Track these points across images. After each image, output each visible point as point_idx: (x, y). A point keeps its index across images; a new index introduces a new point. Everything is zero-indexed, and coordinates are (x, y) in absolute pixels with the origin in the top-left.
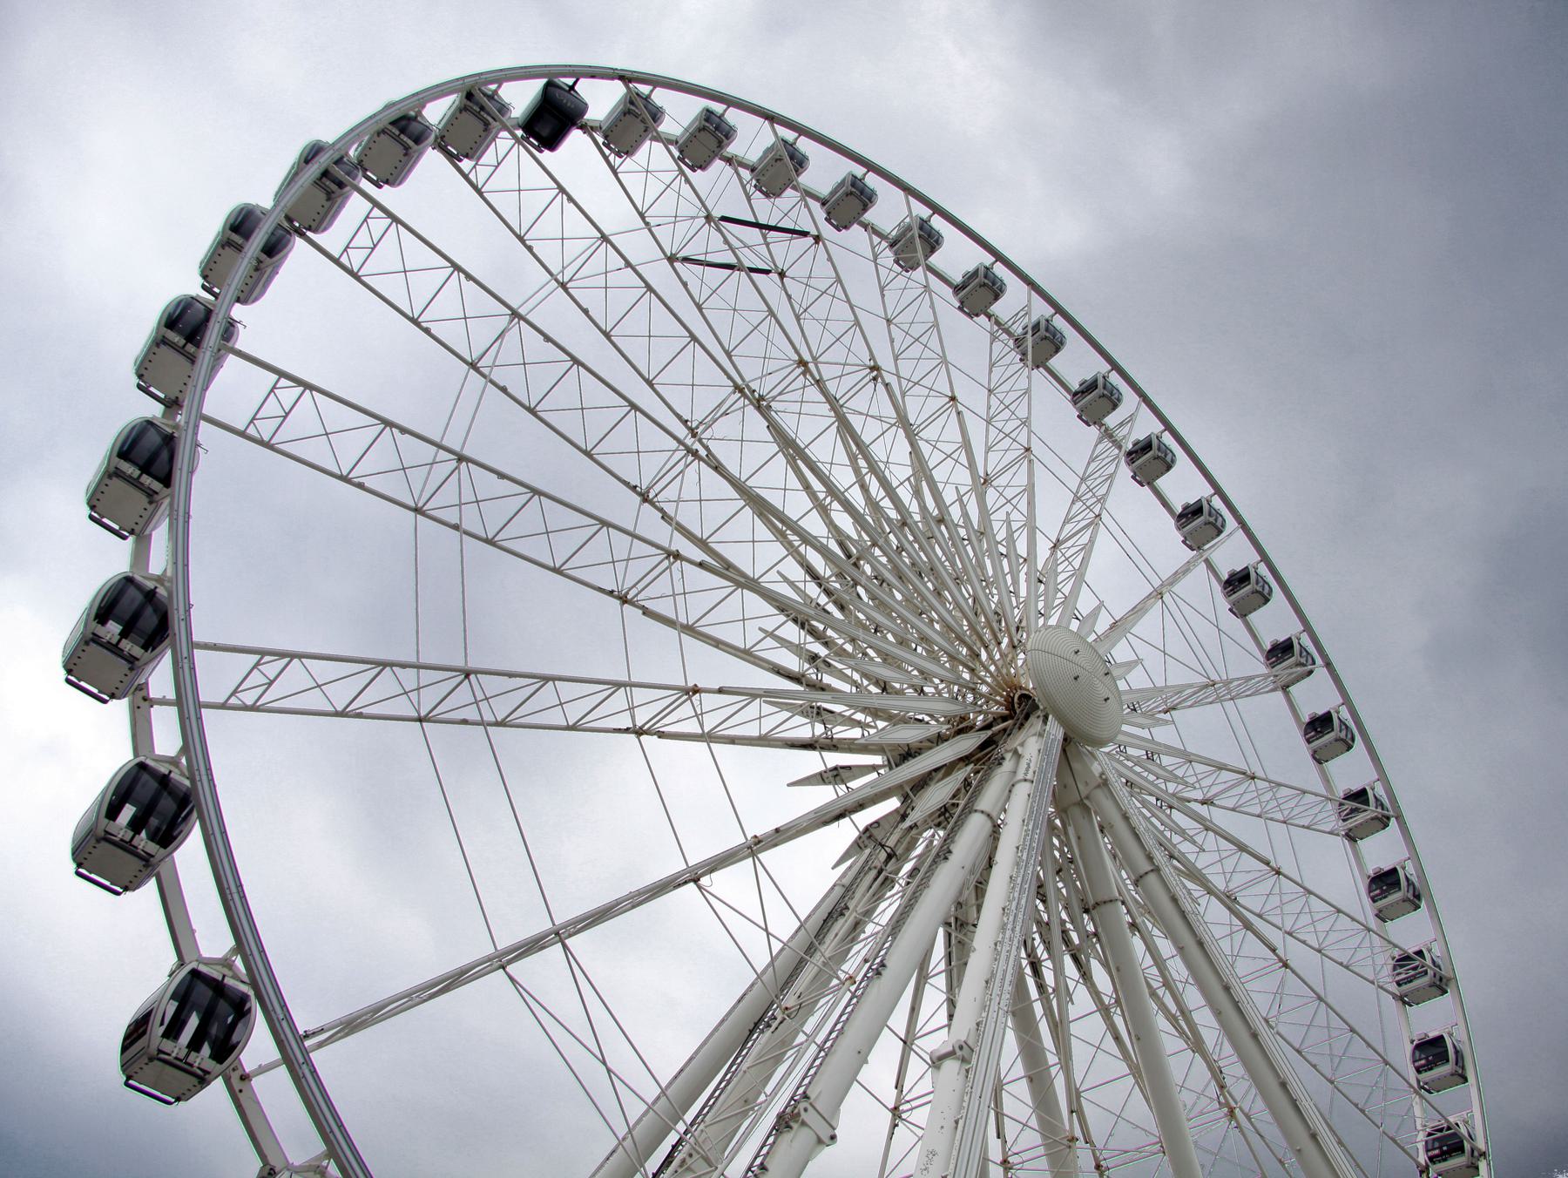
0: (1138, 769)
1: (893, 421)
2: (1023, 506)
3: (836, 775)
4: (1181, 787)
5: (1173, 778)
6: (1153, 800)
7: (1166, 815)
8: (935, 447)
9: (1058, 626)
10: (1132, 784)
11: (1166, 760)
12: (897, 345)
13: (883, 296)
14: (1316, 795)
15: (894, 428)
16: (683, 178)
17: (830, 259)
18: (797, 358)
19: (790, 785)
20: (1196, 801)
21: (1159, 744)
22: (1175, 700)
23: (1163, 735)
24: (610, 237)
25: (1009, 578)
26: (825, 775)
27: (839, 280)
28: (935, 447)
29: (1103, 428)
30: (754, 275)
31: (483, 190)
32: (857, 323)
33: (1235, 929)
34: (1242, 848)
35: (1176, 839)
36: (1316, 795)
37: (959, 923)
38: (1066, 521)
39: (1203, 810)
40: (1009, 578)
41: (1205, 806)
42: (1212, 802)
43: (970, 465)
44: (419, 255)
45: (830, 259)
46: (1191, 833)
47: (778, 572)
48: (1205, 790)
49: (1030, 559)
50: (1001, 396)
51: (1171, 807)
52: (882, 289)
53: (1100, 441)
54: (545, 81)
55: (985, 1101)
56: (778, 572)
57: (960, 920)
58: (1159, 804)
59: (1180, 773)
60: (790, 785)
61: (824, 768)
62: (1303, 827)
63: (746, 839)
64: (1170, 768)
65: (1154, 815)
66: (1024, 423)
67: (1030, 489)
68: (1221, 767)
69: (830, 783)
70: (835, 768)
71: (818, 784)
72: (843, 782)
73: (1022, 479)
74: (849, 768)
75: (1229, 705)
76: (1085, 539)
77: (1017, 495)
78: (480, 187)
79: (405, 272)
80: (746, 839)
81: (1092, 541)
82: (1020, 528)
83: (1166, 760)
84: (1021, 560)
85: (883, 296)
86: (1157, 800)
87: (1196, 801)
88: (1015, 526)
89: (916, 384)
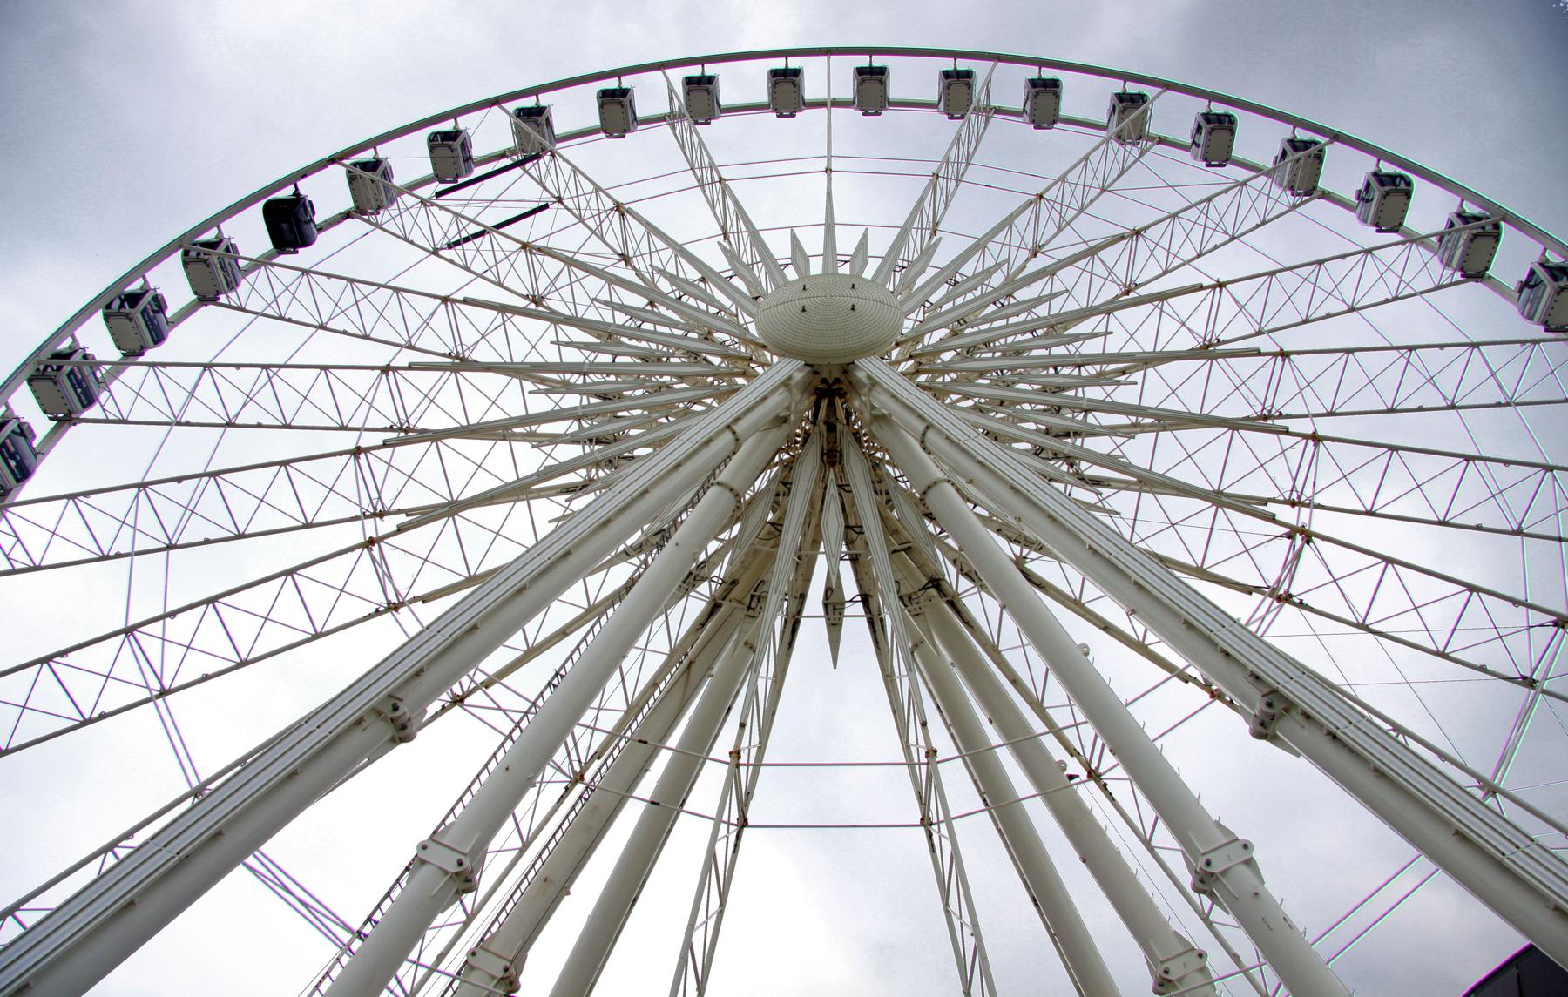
0: (959, 301)
1: (499, 320)
2: (660, 244)
3: (834, 607)
4: (1005, 268)
5: (988, 273)
6: (992, 308)
7: (1014, 305)
8: (571, 284)
9: (825, 274)
10: (963, 319)
11: (968, 269)
12: (457, 260)
13: (412, 243)
14: (1097, 148)
15: (508, 324)
16: (159, 367)
17: (329, 276)
18: (379, 371)
19: (835, 667)
20: (1028, 260)
21: (948, 266)
22: (927, 219)
23: (942, 258)
24: (146, 480)
25: (660, 329)
26: (832, 621)
27: (351, 281)
28: (571, 284)
29: (667, 118)
30: (503, 230)
31: (37, 564)
32: (397, 290)
33: (1160, 306)
34: (1092, 252)
35: (1042, 311)
36: (1097, 148)
37: (906, 599)
38: (713, 207)
39: (1040, 262)
40: (660, 329)
41: (1038, 255)
42: (1040, 246)
43: (587, 271)
44: (275, 637)
45: (329, 276)
46: (1047, 292)
47: (1136, 383)
48: (1023, 245)
49: (707, 275)
50: (567, 195)
51: (1010, 295)
52: (406, 239)
53: (673, 129)
54: (180, 252)
55: (1284, 680)
56: (1136, 383)
57: (905, 595)
58: (1000, 305)
59: (990, 263)
60: (835, 667)
61: (824, 620)
62: (1119, 176)
63: (727, 763)
64: (979, 269)
65: (1007, 317)
66: (596, 192)
67: (651, 229)
68: (1008, 222)
69: (840, 619)
70: (826, 605)
71: (840, 631)
72: (843, 603)
73: (639, 230)
74: (828, 590)
75: (972, 174)
76: (731, 207)
77: (649, 244)
78: (32, 565)
79: (1247, 550)
80: (727, 763)
81: (736, 203)
82: (676, 263)
83: (968, 269)
84: (649, 308)
85: (412, 243)
86: (994, 303)
87: (1028, 260)
88: (671, 269)
89: (496, 265)
